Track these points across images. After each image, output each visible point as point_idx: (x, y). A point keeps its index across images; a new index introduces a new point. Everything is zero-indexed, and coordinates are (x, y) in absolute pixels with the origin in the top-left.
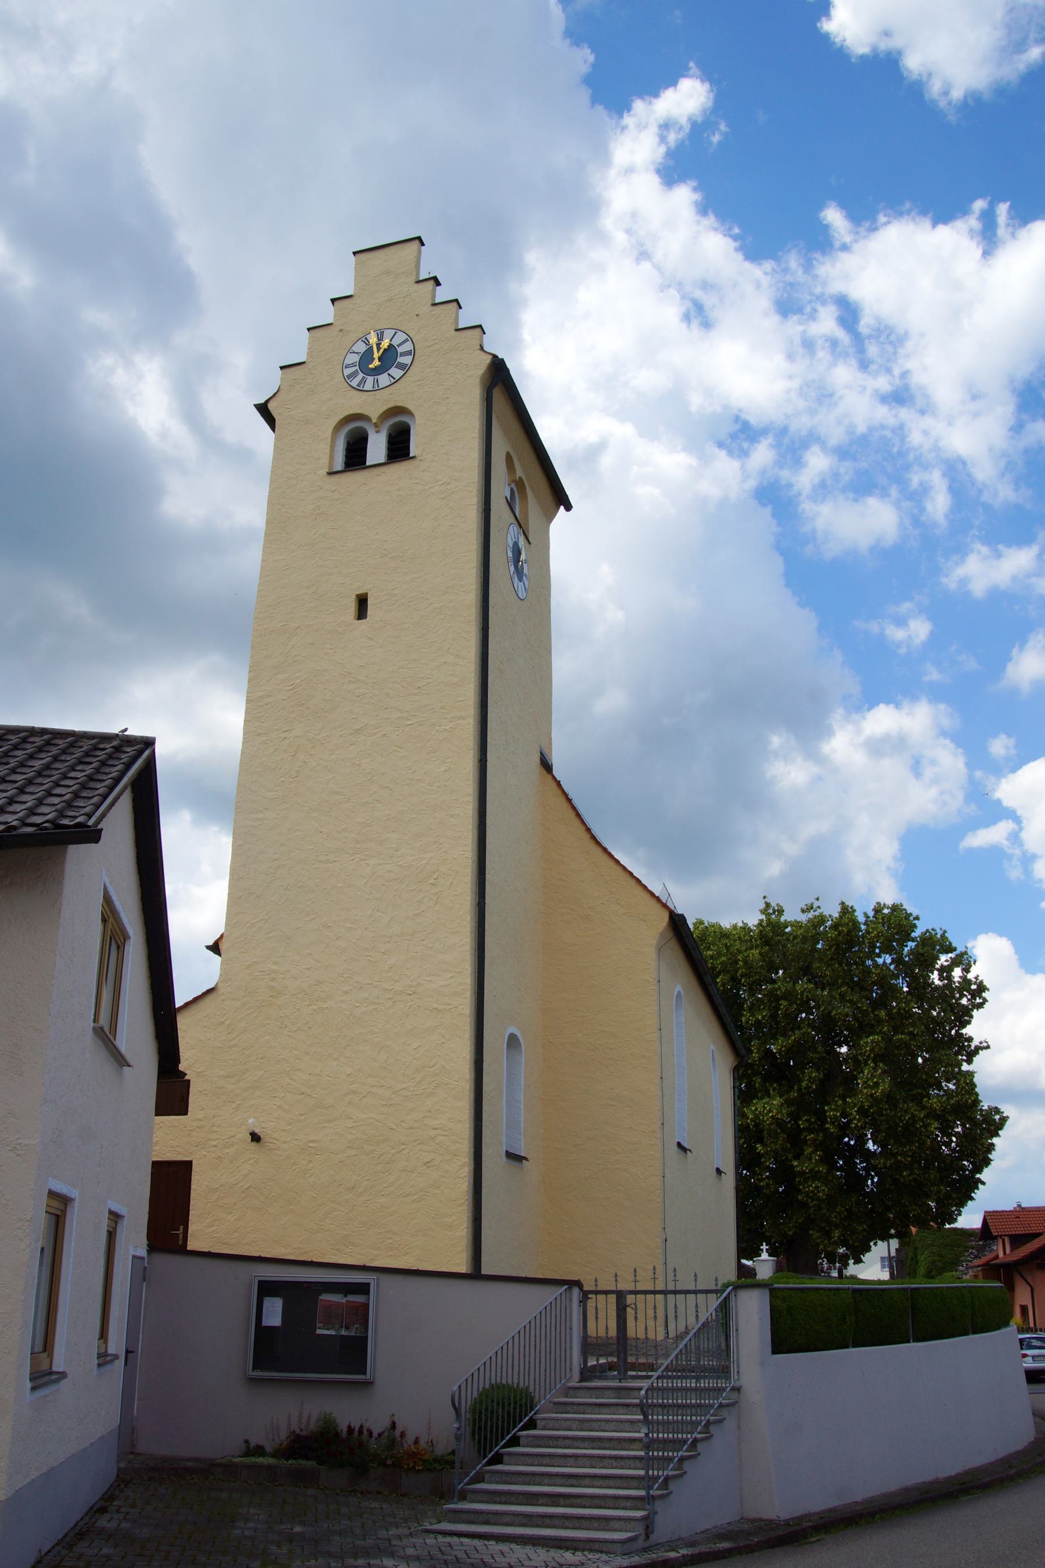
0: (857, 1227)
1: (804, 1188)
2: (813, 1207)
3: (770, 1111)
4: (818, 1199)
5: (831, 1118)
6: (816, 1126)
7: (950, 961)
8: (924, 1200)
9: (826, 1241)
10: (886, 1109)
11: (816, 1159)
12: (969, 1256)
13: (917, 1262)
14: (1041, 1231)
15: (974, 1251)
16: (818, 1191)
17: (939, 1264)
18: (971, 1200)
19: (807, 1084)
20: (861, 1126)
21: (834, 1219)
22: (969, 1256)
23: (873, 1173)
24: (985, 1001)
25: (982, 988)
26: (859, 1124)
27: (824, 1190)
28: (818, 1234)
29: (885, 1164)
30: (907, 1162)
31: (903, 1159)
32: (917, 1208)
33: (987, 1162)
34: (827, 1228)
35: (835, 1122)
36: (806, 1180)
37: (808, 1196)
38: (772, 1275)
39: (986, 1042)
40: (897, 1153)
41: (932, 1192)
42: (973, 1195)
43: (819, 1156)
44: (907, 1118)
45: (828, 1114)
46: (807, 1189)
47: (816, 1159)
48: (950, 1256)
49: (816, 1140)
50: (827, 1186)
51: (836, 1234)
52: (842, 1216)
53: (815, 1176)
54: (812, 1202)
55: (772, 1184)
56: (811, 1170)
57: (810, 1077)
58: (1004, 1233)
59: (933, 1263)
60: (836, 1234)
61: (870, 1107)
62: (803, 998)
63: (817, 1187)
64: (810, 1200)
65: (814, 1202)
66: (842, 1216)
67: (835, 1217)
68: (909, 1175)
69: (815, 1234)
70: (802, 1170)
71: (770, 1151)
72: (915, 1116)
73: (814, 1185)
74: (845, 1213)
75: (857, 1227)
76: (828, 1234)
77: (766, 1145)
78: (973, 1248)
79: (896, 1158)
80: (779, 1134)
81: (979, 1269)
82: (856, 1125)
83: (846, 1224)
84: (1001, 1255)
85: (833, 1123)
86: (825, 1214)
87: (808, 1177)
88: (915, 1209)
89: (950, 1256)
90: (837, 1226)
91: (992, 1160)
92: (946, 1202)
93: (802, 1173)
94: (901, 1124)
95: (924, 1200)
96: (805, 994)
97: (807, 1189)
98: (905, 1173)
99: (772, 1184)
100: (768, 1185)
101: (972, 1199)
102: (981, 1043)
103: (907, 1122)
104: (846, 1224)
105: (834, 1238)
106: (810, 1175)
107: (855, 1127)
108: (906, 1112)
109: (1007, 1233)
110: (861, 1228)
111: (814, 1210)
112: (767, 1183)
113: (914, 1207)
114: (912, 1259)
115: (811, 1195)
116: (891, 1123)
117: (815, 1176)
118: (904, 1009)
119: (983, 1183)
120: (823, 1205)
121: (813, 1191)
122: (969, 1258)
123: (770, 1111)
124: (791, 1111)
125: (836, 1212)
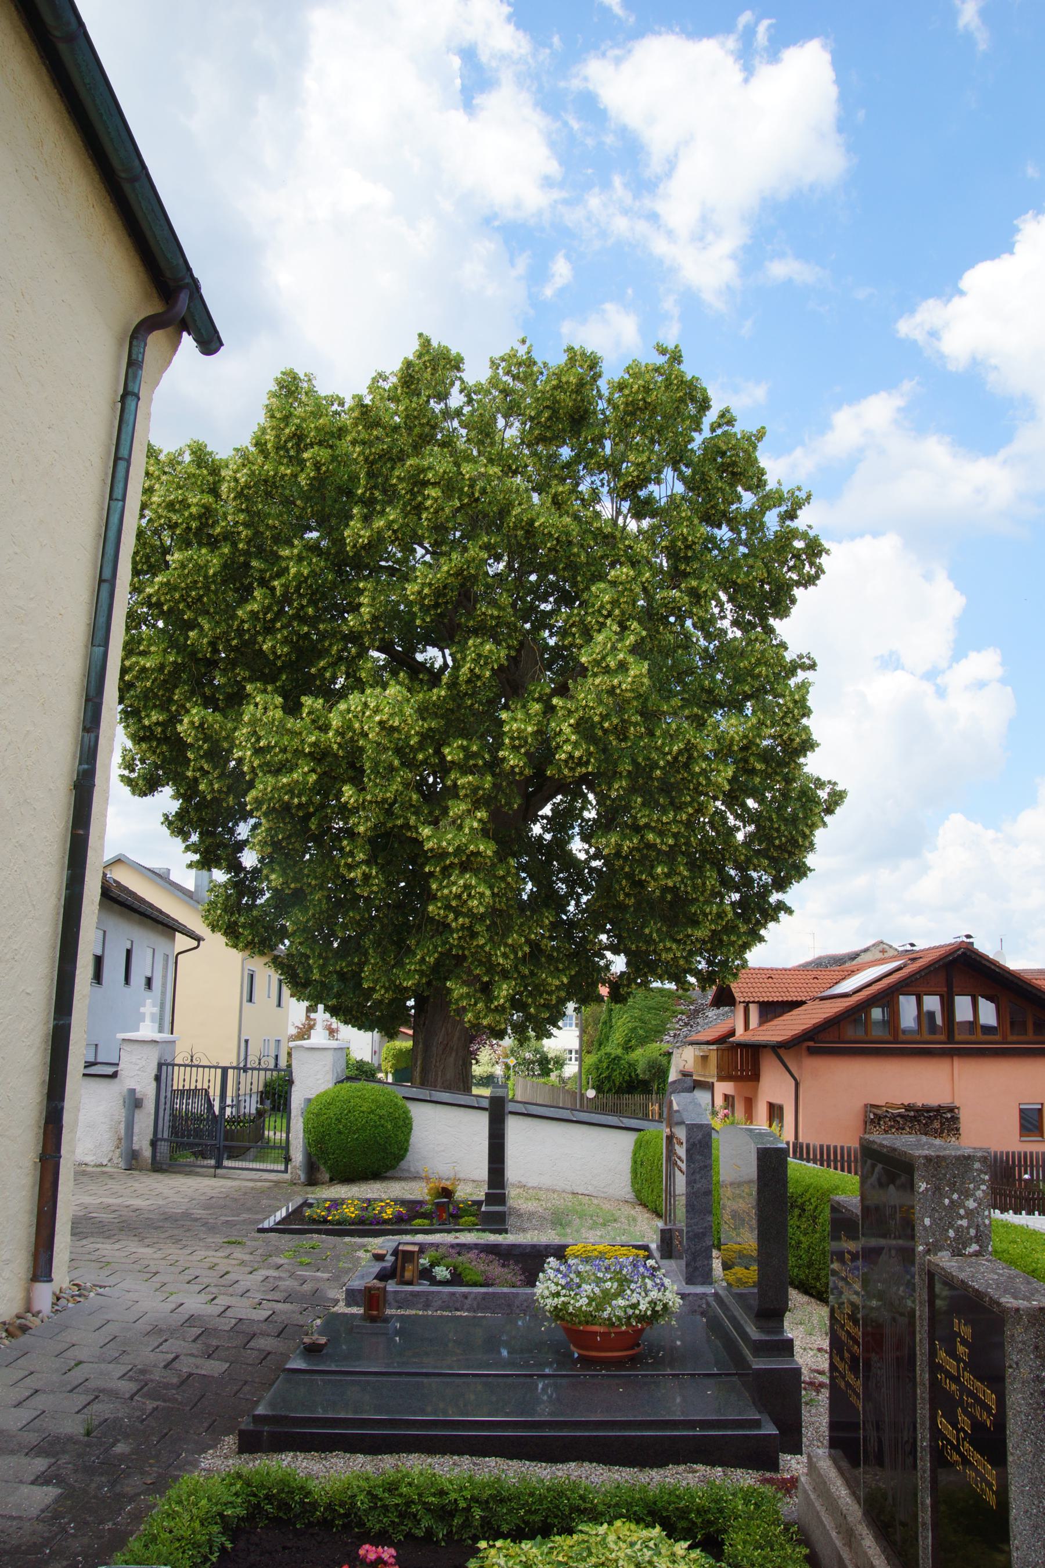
0: (549, 980)
1: (441, 888)
2: (458, 931)
3: (377, 711)
4: (470, 913)
5: (512, 739)
6: (480, 762)
7: (390, 1258)
8: (690, 931)
9: (480, 1005)
10: (636, 724)
11: (471, 828)
12: (677, 1022)
13: (611, 1027)
14: (804, 999)
15: (684, 1017)
16: (469, 895)
17: (641, 1032)
18: (760, 942)
19: (471, 670)
20: (581, 758)
21: (501, 961)
22: (677, 1022)
23: (579, 890)
24: (820, 570)
25: (815, 549)
26: (577, 754)
27: (482, 895)
28: (465, 990)
29: (619, 846)
30: (664, 847)
31: (658, 841)
32: (674, 946)
33: (801, 871)
34: (486, 979)
35: (521, 746)
36: (446, 871)
37: (448, 907)
38: (330, 1085)
39: (809, 658)
40: (647, 826)
41: (705, 915)
42: (762, 932)
43: (480, 820)
44: (676, 748)
45: (506, 729)
46: (446, 891)
47: (471, 828)
48: (653, 1022)
49: (478, 788)
50: (491, 888)
51: (504, 991)
52: (520, 954)
53: (468, 863)
54: (456, 919)
55: (376, 877)
56: (459, 850)
57: (479, 656)
58: (752, 999)
59: (634, 1030)
60: (504, 991)
61: (604, 717)
62: (473, 493)
63: (467, 887)
64: (451, 916)
65: (461, 920)
66: (520, 954)
67: (505, 955)
68: (668, 876)
69: (457, 989)
70: (440, 847)
71: (371, 802)
72: (694, 747)
73: (461, 882)
74: (527, 949)
75: (549, 980)
76: (486, 990)
77: (364, 789)
78: (682, 1013)
79: (642, 836)
80: (397, 770)
81: (714, 1047)
82: (571, 756)
83: (527, 972)
84: (740, 1030)
85: (515, 748)
86: (482, 947)
87: (452, 864)
88: (670, 949)
89: (653, 1022)
90: (505, 975)
91: (811, 870)
92: (725, 938)
93: (441, 855)
94: (662, 763)
95: (690, 931)
96: (480, 484)
97: (446, 891)
98: (659, 870)
99: (376, 877)
100: (366, 877)
101: (761, 939)
102: (800, 657)
103: (675, 758)
104: (527, 972)
105: (497, 998)
106: (456, 861)
107: (566, 761)
108: (673, 737)
109: (757, 999)
110: (557, 983)
111: (460, 938)
112: (364, 874)
113: (668, 945)
114: (605, 1023)
115: (454, 903)
116: (640, 760)
117: (468, 863)
118: (685, 539)
119: (789, 911)
120: (478, 928)
121: (458, 897)
122: (677, 1026)
123: (377, 711)
124: (430, 729)
125: (506, 945)
